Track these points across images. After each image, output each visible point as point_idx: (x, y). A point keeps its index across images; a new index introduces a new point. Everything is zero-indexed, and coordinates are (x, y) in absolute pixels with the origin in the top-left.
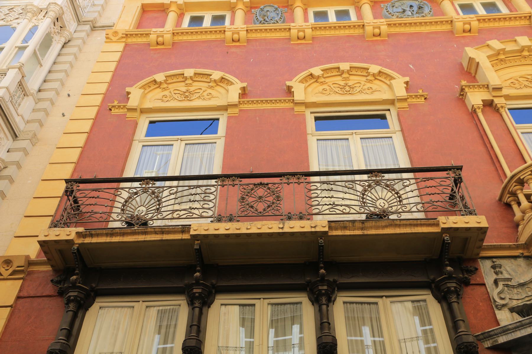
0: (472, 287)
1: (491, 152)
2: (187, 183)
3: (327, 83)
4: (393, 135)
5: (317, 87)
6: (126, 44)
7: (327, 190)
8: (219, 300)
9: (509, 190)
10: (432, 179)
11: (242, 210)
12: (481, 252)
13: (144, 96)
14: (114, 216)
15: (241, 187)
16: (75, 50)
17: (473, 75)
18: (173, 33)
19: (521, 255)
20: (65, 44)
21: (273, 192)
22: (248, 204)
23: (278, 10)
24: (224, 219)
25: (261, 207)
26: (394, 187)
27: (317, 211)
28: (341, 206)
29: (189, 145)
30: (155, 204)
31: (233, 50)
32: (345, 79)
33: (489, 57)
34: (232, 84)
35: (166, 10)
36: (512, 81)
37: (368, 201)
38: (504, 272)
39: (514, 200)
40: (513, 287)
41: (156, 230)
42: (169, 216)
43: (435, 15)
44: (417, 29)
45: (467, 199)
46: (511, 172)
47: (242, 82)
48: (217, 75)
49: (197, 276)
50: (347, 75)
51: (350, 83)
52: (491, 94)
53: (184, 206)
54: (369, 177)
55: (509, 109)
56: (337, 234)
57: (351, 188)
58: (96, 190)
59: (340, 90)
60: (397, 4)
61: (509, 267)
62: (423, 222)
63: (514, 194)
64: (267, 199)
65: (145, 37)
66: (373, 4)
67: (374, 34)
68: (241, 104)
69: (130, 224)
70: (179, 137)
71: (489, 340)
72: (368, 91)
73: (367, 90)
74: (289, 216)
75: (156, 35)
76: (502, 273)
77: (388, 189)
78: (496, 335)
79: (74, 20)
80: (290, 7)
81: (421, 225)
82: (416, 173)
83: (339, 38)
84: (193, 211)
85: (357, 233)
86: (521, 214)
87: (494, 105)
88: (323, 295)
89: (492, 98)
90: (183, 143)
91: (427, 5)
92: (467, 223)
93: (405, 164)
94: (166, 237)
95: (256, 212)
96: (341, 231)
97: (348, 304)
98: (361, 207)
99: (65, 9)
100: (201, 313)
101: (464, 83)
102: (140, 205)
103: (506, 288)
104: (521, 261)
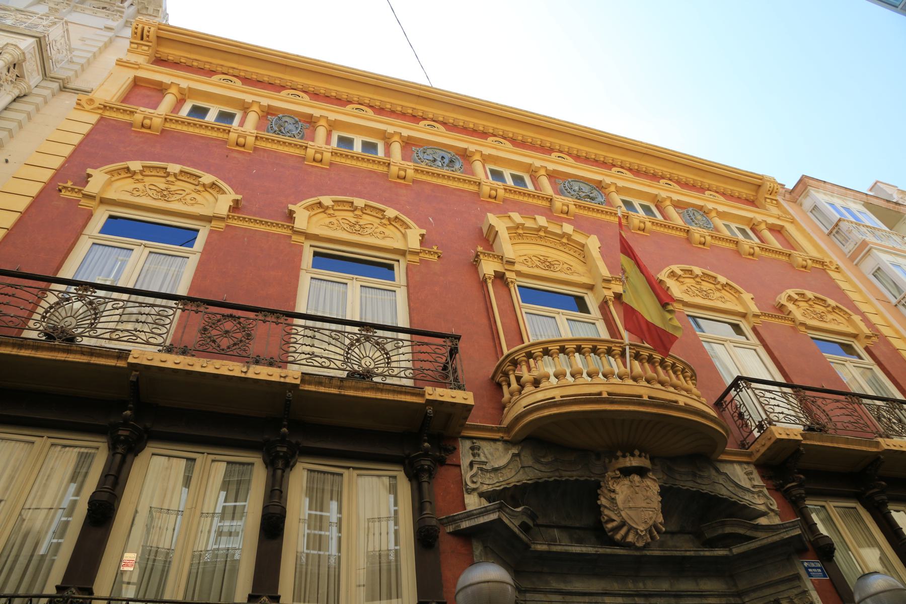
0: (447, 467)
1: (493, 327)
2: (141, 299)
4: (397, 290)
5: (323, 219)
8: (149, 449)
10: (427, 344)
11: (201, 343)
13: (109, 183)
14: (31, 324)
15: (206, 316)
16: (30, 108)
17: (491, 243)
18: (166, 119)
19: (501, 439)
20: (18, 97)
21: (244, 328)
22: (210, 337)
24: (175, 350)
25: (225, 342)
30: (90, 317)
31: (235, 155)
33: (508, 228)
35: (164, 91)
36: (526, 257)
37: (352, 357)
38: (482, 455)
39: (506, 381)
40: (487, 471)
41: (83, 349)
42: (107, 336)
44: (445, 182)
46: (508, 350)
47: (236, 193)
48: (207, 178)
50: (360, 213)
51: (362, 222)
52: (504, 267)
53: (130, 326)
55: (519, 286)
56: (310, 389)
57: (337, 340)
58: (12, 286)
59: (349, 227)
60: (429, 151)
62: (408, 390)
63: (506, 375)
64: (233, 335)
66: (404, 144)
68: (230, 218)
69: (50, 337)
70: (144, 242)
72: (379, 236)
73: (378, 234)
74: (257, 360)
75: (143, 116)
76: (479, 455)
77: (378, 347)
78: (460, 519)
79: (38, 72)
80: (313, 124)
81: (406, 393)
82: (414, 336)
83: (359, 170)
85: (332, 392)
86: (509, 396)
87: (505, 278)
89: (504, 271)
90: (147, 250)
91: (458, 160)
92: (442, 396)
93: (403, 322)
95: (218, 349)
98: (344, 362)
99: (28, 56)
100: (123, 461)
101: (480, 249)
102: (69, 315)
103: (480, 472)
104: (500, 445)
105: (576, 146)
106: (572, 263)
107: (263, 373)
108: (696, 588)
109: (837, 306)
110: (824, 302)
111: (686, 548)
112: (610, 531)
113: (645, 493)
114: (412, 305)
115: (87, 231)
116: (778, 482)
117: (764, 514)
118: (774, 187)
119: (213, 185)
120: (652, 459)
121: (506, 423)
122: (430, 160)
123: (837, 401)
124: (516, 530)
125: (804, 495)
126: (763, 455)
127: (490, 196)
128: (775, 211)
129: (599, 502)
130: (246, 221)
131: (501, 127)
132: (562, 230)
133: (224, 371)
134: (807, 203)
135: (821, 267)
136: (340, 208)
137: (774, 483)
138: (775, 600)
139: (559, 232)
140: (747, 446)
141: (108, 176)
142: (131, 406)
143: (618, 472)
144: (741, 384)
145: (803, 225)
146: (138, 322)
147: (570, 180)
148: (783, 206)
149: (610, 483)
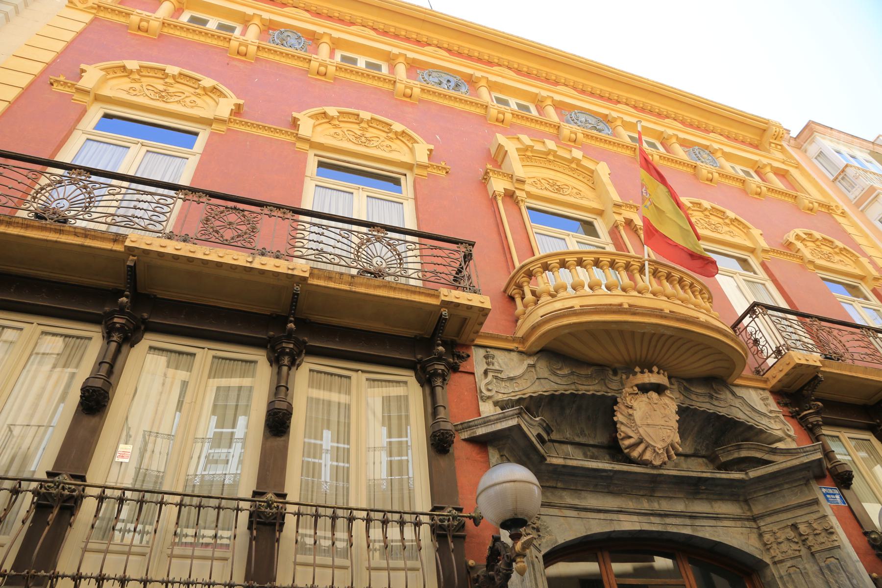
0: (459, 374)
2: (141, 187)
3: (341, 128)
4: (405, 202)
6: (96, 18)
7: (316, 234)
8: (149, 340)
9: (516, 282)
10: (440, 249)
11: (203, 232)
12: (477, 340)
13: (104, 81)
15: (209, 207)
17: (499, 164)
18: (163, 23)
19: (515, 349)
21: (248, 220)
22: (212, 228)
23: (301, 39)
25: (228, 234)
26: (397, 247)
27: (299, 254)
28: (330, 255)
29: (151, 153)
30: (84, 201)
31: (236, 63)
32: (363, 129)
33: (518, 150)
34: (225, 96)
37: (363, 256)
38: (496, 364)
40: (502, 379)
41: (77, 230)
42: (103, 220)
43: (471, 95)
44: (451, 104)
45: (474, 278)
48: (207, 82)
49: (122, 302)
51: (368, 135)
52: (513, 185)
54: (370, 231)
55: (529, 208)
56: (319, 284)
57: (347, 238)
59: (354, 139)
60: (434, 74)
61: (502, 359)
63: (520, 287)
64: (238, 227)
65: (124, 16)
67: (141, 27)
68: (231, 122)
69: (38, 217)
71: (467, 431)
72: (386, 149)
73: (385, 147)
75: (140, 18)
76: (493, 364)
77: (389, 248)
84: (136, 220)
85: (342, 288)
87: (515, 196)
88: (287, 354)
89: (514, 189)
90: (145, 149)
93: (411, 225)
94: (88, 242)
95: (221, 239)
96: (325, 281)
97: (315, 373)
100: (118, 351)
101: (489, 166)
102: (61, 197)
103: (494, 380)
104: (514, 355)
105: (581, 81)
106: (581, 189)
107: (270, 264)
108: (711, 511)
109: (844, 248)
110: (831, 243)
111: (698, 469)
112: (626, 449)
113: (663, 411)
114: (420, 216)
115: (82, 125)
116: (794, 409)
117: (780, 440)
118: (779, 132)
119: (214, 89)
120: (669, 378)
121: (520, 334)
122: (436, 83)
123: (853, 333)
124: (533, 439)
125: (821, 423)
126: (780, 381)
127: (497, 120)
128: (779, 155)
129: (615, 419)
130: (249, 126)
131: (506, 57)
132: (571, 155)
133: (228, 260)
134: (813, 150)
135: (826, 211)
136: (345, 120)
137: (790, 410)
138: (792, 525)
139: (568, 156)
140: (762, 373)
141: (103, 73)
142: (128, 293)
143: (636, 388)
144: (757, 310)
145: (807, 169)
146: (136, 209)
147: (576, 111)
148: (788, 151)
149: (627, 399)
